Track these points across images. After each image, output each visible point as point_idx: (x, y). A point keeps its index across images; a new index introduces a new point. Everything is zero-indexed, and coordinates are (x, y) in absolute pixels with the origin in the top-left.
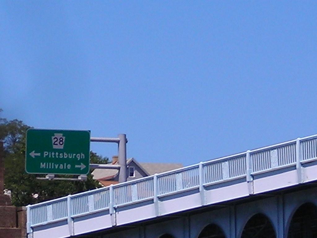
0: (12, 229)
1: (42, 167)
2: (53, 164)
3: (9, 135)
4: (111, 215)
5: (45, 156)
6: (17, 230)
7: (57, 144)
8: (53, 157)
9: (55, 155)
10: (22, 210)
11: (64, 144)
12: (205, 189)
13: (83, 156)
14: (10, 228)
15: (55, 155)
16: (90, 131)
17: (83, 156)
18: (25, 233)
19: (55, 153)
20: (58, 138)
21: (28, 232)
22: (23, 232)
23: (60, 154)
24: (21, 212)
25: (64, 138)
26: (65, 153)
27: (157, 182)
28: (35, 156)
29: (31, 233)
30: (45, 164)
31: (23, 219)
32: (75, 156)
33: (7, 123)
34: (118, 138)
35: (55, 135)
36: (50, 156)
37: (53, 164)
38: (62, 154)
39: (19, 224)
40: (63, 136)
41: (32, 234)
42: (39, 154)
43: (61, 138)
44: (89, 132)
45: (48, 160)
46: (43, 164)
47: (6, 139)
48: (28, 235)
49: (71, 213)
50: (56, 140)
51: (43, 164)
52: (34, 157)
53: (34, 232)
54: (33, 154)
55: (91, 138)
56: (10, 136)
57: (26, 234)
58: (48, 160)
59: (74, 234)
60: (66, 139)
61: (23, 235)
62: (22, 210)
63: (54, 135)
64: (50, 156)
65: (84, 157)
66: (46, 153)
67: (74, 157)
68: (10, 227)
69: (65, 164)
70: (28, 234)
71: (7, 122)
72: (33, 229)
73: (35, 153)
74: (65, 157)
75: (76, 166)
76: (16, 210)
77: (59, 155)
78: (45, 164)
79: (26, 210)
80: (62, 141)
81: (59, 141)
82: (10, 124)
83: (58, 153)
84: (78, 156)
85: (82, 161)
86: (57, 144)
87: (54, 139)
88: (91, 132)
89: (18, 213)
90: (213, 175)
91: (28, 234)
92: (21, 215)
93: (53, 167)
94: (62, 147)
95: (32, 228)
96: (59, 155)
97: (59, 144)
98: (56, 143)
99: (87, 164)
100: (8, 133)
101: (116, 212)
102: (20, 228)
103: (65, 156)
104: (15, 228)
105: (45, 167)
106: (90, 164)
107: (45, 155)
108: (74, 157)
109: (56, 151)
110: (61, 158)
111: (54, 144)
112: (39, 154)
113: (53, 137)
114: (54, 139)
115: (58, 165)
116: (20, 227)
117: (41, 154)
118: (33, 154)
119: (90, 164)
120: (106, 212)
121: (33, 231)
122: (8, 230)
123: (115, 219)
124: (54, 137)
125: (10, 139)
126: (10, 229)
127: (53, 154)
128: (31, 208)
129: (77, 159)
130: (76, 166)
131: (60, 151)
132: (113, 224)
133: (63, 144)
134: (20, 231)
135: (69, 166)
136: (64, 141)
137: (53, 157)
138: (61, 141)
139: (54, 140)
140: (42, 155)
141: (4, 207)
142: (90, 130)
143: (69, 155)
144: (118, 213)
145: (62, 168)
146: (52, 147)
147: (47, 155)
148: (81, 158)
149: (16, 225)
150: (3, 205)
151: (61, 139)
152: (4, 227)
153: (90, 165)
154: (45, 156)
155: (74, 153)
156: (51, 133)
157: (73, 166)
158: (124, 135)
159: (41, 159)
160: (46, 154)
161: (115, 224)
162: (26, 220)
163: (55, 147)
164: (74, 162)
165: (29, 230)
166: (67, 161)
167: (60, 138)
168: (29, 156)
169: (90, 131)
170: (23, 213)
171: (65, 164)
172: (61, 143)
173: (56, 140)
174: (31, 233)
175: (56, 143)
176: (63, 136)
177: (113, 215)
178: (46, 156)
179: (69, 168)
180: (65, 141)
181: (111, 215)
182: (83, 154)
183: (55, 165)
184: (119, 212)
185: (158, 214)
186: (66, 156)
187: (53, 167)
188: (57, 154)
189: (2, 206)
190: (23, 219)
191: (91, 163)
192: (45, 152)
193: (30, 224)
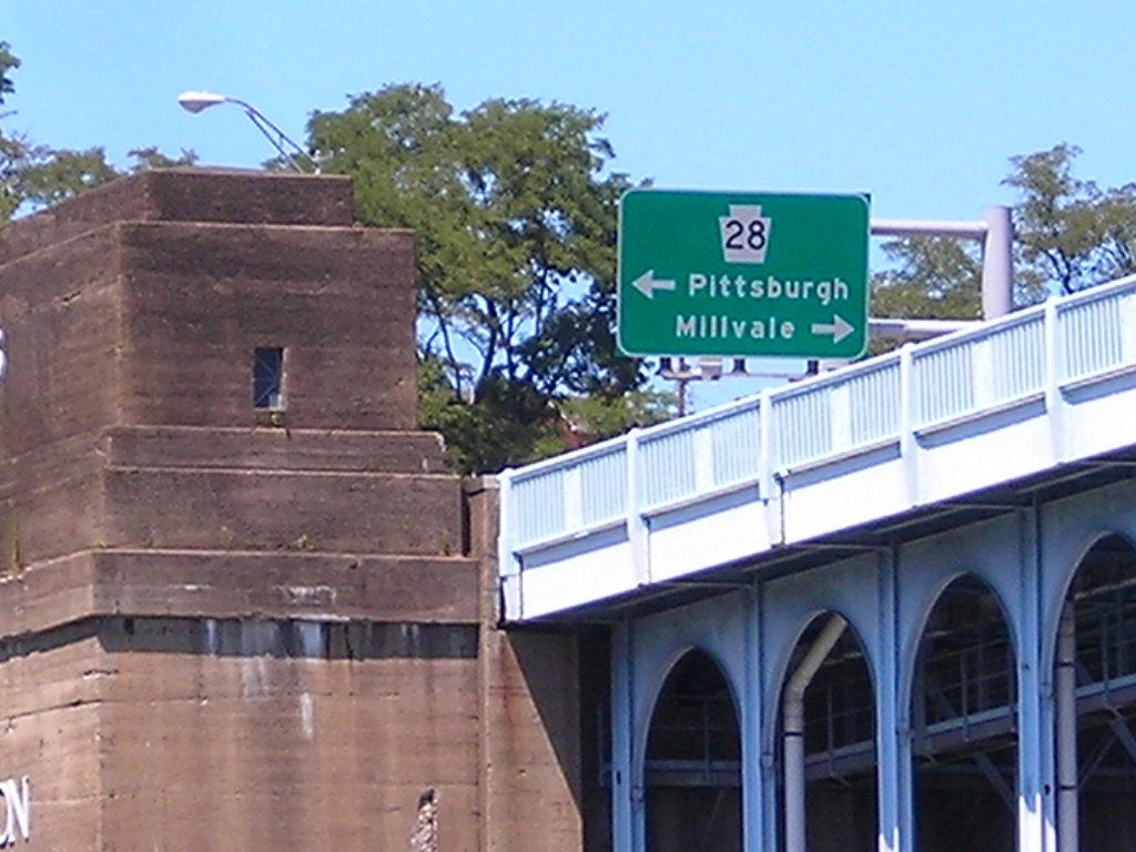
0: (445, 562)
1: (682, 333)
2: (724, 319)
3: (1108, 241)
4: (766, 502)
5: (692, 293)
6: (469, 563)
7: (740, 247)
8: (726, 293)
9: (732, 288)
10: (482, 490)
11: (769, 247)
12: (1066, 400)
13: (841, 291)
14: (438, 558)
15: (732, 288)
16: (868, 196)
17: (841, 291)
18: (491, 578)
19: (732, 280)
20: (742, 222)
21: (503, 573)
22: (486, 573)
23: (754, 285)
24: (479, 496)
25: (767, 222)
26: (771, 279)
27: (912, 375)
28: (655, 291)
29: (514, 576)
30: (693, 319)
31: (485, 524)
32: (812, 291)
33: (1101, 199)
34: (979, 219)
35: (732, 212)
36: (713, 293)
37: (724, 319)
38: (761, 283)
39: (473, 540)
40: (763, 215)
41: (518, 578)
42: (671, 285)
43: (755, 223)
44: (865, 200)
45: (702, 306)
46: (686, 321)
47: (1095, 255)
48: (505, 585)
49: (639, 498)
50: (736, 229)
51: (686, 321)
52: (650, 296)
53: (527, 573)
54: (646, 284)
55: (874, 222)
56: (1112, 246)
57: (498, 581)
58: (702, 306)
59: (650, 577)
60: (773, 224)
61: (485, 583)
62: (482, 490)
63: (728, 214)
64: (713, 293)
65: (845, 296)
66: (698, 281)
67: (805, 295)
68: (437, 554)
69: (772, 320)
70: (503, 579)
71: (1101, 194)
72: (521, 562)
73: (655, 278)
74: (771, 294)
75: (817, 328)
76: (463, 492)
77: (747, 289)
78: (693, 319)
79: (498, 490)
80: (759, 234)
81: (747, 233)
82: (1109, 202)
83: (744, 278)
84: (823, 290)
85: (837, 307)
86: (740, 247)
87: (729, 226)
88: (873, 198)
89: (470, 500)
90: (1109, 334)
91: (503, 579)
92: (479, 506)
93: (724, 333)
94: (759, 257)
95: (519, 557)
96: (747, 289)
97: (746, 246)
98: (734, 242)
99: (859, 324)
100: (1106, 235)
101: (783, 491)
102: (476, 559)
103: (770, 290)
104: (459, 557)
105: (693, 334)
106: (871, 320)
107: (693, 287)
108: (805, 295)
109: (734, 270)
110: (757, 299)
111: (729, 245)
112: (671, 285)
113: (723, 221)
114: (729, 226)
115: (743, 324)
116: (478, 552)
117: (678, 284)
118: (646, 284)
119: (871, 320)
120: (749, 493)
121: (522, 569)
122: (426, 563)
123: (779, 517)
124: (729, 220)
125: (1109, 255)
126: (438, 562)
127: (725, 281)
128: (515, 482)
129: (821, 300)
130: (817, 328)
131: (752, 272)
132: (773, 538)
133: (764, 248)
134: (477, 567)
135: (788, 329)
136: (765, 234)
137: (726, 293)
138: (754, 234)
139: (728, 230)
140: (683, 285)
141: (415, 479)
142: (867, 191)
143: (788, 284)
144: (790, 497)
145: (761, 335)
146: (722, 257)
147: (700, 286)
148: (836, 296)
149: (459, 544)
150: (413, 472)
151: (757, 228)
152: (411, 554)
153: (871, 325)
154: (692, 293)
155: (809, 280)
156: (715, 204)
157: (802, 329)
158: (1004, 212)
159: (678, 302)
160: (696, 281)
161: (778, 540)
162: (498, 526)
163: (730, 256)
164: (810, 310)
165: (507, 565)
166: (781, 308)
167: (750, 222)
168: (632, 295)
169: (868, 196)
170: (485, 499)
171: (772, 320)
172: (757, 240)
173: (736, 229)
174: (514, 576)
175: (734, 242)
176: (763, 215)
177: (770, 503)
178: (697, 291)
179: (788, 336)
180: (771, 236)
181: (766, 502)
182: (842, 280)
183: (735, 324)
184: (794, 493)
185: (916, 499)
186: (775, 289)
187: (724, 333)
188: (740, 282)
189: (408, 475)
190: (485, 524)
191: (877, 316)
192: (693, 277)
193: (511, 540)
